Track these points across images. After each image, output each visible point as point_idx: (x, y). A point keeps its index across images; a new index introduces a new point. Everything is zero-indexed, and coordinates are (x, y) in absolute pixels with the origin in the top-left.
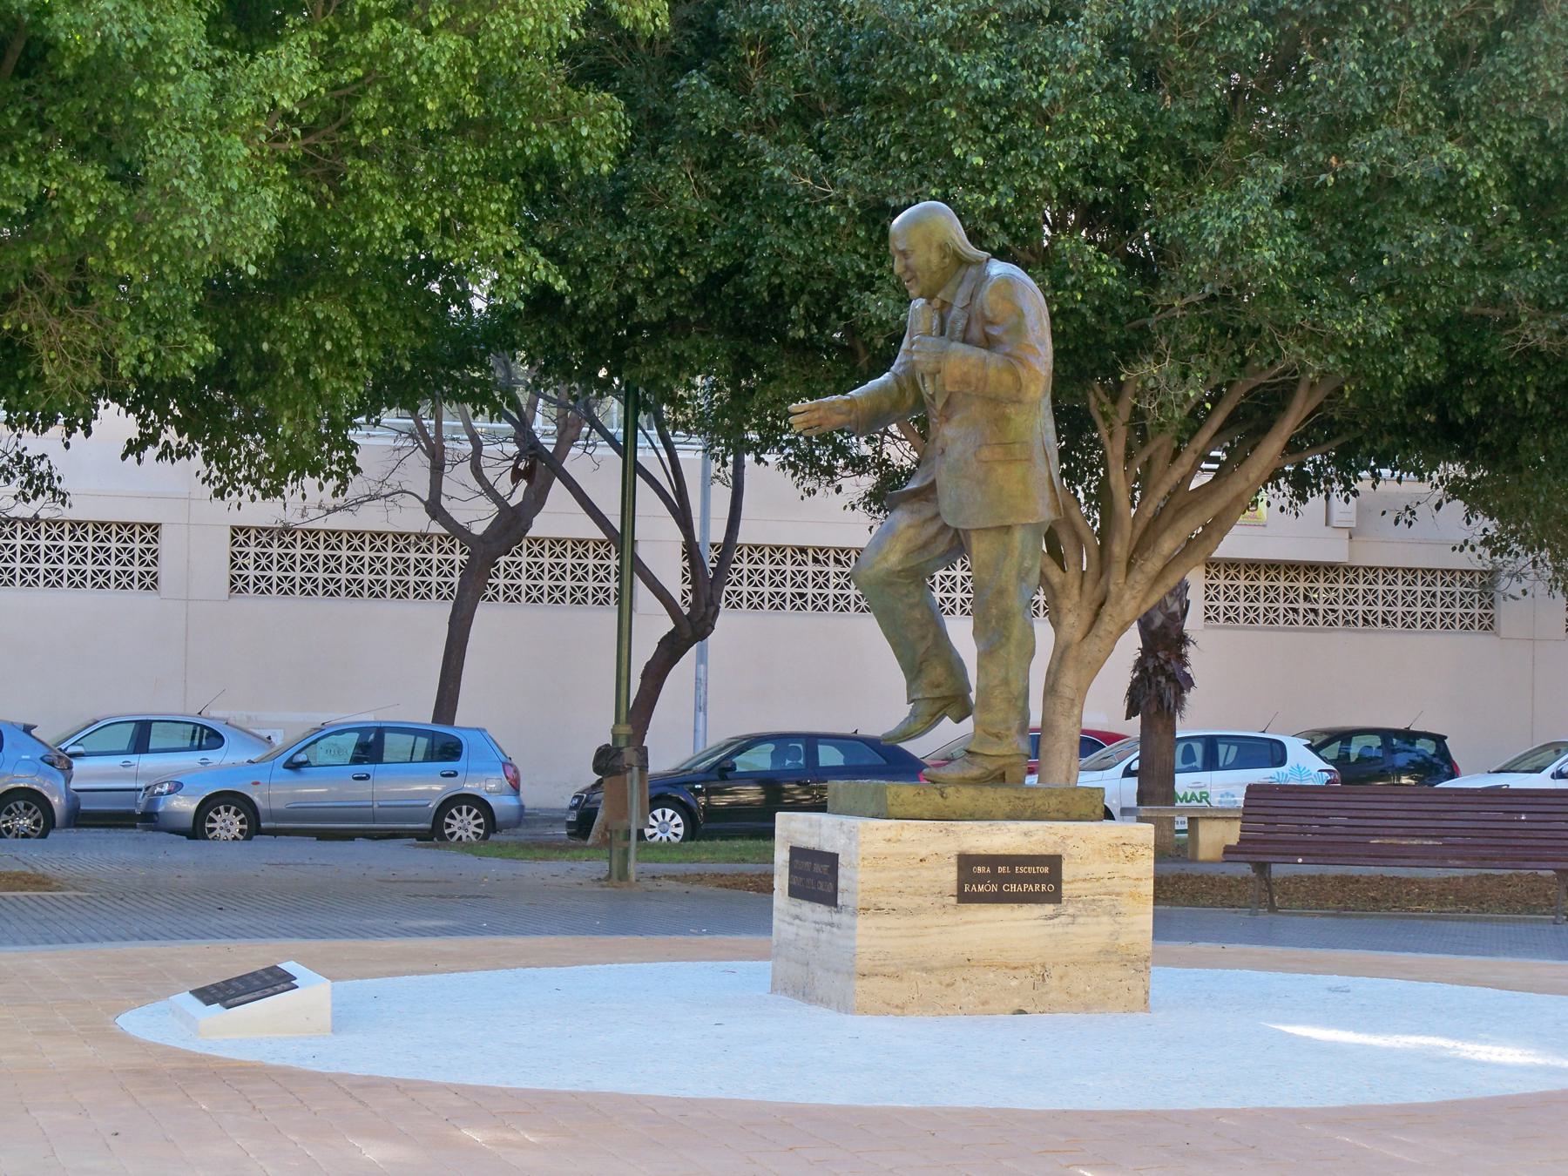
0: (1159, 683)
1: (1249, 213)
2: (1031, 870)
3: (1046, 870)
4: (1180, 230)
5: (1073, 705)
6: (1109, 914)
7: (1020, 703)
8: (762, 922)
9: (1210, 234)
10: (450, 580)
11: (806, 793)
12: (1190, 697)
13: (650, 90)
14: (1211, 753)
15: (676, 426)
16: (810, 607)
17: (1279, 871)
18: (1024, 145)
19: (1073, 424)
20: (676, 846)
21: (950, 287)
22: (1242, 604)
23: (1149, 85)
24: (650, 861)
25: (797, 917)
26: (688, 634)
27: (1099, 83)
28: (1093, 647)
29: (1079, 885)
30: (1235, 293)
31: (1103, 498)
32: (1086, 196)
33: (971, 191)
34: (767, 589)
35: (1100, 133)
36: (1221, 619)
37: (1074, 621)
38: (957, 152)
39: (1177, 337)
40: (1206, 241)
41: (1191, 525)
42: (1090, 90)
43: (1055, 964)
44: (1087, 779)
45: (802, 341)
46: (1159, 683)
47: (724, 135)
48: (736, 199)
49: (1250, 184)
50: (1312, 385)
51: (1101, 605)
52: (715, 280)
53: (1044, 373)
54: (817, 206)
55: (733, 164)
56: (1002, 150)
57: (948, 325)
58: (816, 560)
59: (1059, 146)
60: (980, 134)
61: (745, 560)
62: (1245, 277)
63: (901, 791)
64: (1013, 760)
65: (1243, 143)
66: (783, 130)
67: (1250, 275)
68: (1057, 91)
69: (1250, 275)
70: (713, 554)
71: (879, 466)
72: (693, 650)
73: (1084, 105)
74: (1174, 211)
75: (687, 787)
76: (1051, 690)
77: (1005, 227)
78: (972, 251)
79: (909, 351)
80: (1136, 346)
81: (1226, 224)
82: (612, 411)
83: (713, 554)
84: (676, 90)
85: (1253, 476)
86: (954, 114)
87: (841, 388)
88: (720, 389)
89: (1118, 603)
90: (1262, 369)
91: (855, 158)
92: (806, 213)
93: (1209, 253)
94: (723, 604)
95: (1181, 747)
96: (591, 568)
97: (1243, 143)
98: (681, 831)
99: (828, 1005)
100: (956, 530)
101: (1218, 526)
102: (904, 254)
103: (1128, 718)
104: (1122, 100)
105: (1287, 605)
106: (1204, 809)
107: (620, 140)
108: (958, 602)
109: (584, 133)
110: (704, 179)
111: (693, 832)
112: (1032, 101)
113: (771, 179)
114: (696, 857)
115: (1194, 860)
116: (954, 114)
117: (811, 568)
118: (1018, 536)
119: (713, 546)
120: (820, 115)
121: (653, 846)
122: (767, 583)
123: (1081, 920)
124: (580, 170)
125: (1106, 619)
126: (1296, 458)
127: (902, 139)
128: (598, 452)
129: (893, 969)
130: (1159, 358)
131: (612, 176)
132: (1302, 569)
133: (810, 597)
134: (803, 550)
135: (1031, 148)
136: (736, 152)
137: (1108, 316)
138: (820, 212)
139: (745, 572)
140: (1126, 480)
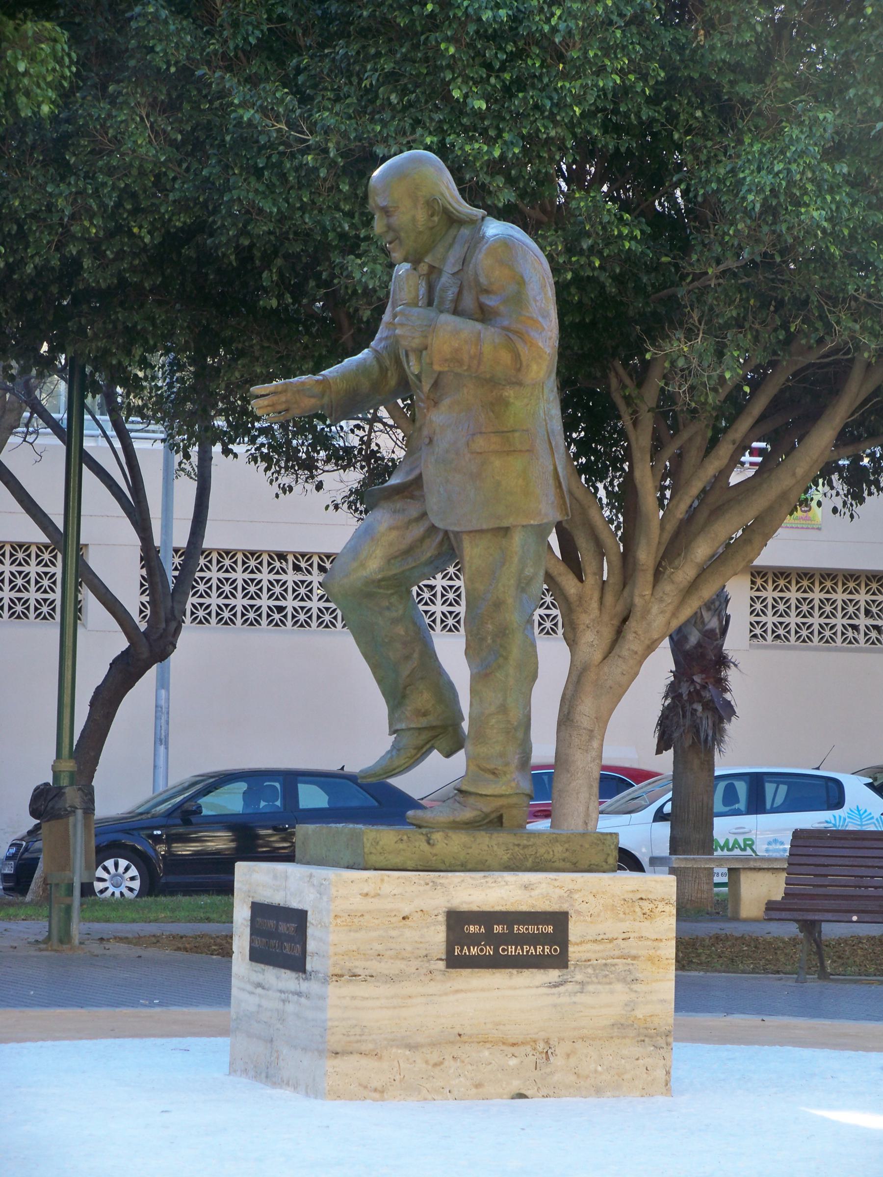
0: (696, 710)
1: (794, 167)
2: (532, 929)
3: (550, 929)
4: (714, 186)
5: (591, 738)
6: (624, 980)
7: (520, 735)
8: (220, 992)
9: (749, 191)
10: (456, 609)
11: (284, 840)
12: (732, 728)
13: (100, 19)
14: (756, 793)
15: (131, 410)
16: (289, 623)
17: (832, 931)
18: (533, 86)
19: (589, 409)
20: (131, 902)
21: (440, 249)
22: (793, 620)
23: (681, 17)
24: (98, 920)
25: (259, 985)
26: (144, 652)
27: (621, 15)
28: (616, 669)
29: (589, 946)
30: (778, 259)
31: (626, 499)
32: (606, 146)
33: (472, 139)
34: (239, 602)
35: (622, 72)
36: (770, 637)
37: (593, 640)
38: (456, 94)
39: (711, 309)
40: (744, 199)
41: (729, 528)
42: (611, 23)
43: (561, 1040)
44: (606, 824)
45: (274, 312)
46: (696, 710)
47: (186, 72)
48: (198, 146)
49: (796, 132)
50: (869, 365)
51: (625, 620)
52: (174, 240)
53: (548, 350)
54: (293, 156)
55: (196, 107)
56: (508, 91)
57: (437, 294)
58: (297, 568)
59: (575, 87)
60: (483, 73)
61: (214, 568)
62: (790, 240)
63: (383, 838)
64: (514, 800)
65: (788, 85)
66: (255, 67)
67: (796, 238)
68: (572, 24)
69: (796, 238)
70: (177, 560)
71: (367, 459)
72: (152, 673)
73: (603, 40)
74: (707, 163)
75: (144, 833)
76: (566, 720)
77: (511, 181)
78: (465, 208)
79: (392, 325)
80: (663, 319)
81: (767, 180)
82: (55, 393)
83: (177, 560)
84: (131, 19)
85: (800, 471)
86: (452, 50)
87: (315, 371)
88: (181, 368)
89: (643, 618)
90: (810, 348)
91: (337, 100)
92: (280, 164)
93: (747, 213)
94: (188, 619)
95: (721, 786)
96: (33, 576)
97: (788, 85)
98: (136, 885)
99: (295, 1088)
100: (446, 532)
101: (761, 529)
102: (386, 212)
103: (659, 751)
104: (649, 35)
105: (846, 621)
106: (747, 859)
107: (63, 77)
108: (439, 616)
109: (21, 67)
110: (162, 122)
111: (151, 886)
112: (543, 35)
113: (239, 123)
114: (152, 916)
115: (736, 918)
116: (452, 50)
117: (291, 577)
118: (517, 539)
119: (176, 551)
120: (298, 50)
121: (106, 903)
122: (239, 594)
123: (591, 988)
124: (16, 112)
125: (630, 636)
126: (850, 450)
127: (391, 78)
128: (40, 441)
129: (371, 1046)
130: (690, 334)
131: (54, 118)
132: (863, 580)
133: (289, 610)
134: (282, 556)
135: (542, 90)
136: (199, 91)
137: (631, 285)
138: (296, 162)
139: (214, 582)
140: (653, 475)
